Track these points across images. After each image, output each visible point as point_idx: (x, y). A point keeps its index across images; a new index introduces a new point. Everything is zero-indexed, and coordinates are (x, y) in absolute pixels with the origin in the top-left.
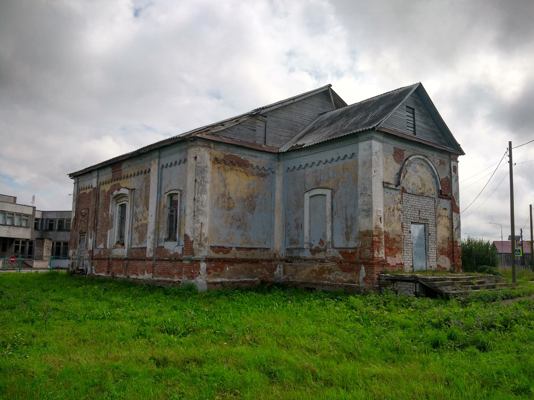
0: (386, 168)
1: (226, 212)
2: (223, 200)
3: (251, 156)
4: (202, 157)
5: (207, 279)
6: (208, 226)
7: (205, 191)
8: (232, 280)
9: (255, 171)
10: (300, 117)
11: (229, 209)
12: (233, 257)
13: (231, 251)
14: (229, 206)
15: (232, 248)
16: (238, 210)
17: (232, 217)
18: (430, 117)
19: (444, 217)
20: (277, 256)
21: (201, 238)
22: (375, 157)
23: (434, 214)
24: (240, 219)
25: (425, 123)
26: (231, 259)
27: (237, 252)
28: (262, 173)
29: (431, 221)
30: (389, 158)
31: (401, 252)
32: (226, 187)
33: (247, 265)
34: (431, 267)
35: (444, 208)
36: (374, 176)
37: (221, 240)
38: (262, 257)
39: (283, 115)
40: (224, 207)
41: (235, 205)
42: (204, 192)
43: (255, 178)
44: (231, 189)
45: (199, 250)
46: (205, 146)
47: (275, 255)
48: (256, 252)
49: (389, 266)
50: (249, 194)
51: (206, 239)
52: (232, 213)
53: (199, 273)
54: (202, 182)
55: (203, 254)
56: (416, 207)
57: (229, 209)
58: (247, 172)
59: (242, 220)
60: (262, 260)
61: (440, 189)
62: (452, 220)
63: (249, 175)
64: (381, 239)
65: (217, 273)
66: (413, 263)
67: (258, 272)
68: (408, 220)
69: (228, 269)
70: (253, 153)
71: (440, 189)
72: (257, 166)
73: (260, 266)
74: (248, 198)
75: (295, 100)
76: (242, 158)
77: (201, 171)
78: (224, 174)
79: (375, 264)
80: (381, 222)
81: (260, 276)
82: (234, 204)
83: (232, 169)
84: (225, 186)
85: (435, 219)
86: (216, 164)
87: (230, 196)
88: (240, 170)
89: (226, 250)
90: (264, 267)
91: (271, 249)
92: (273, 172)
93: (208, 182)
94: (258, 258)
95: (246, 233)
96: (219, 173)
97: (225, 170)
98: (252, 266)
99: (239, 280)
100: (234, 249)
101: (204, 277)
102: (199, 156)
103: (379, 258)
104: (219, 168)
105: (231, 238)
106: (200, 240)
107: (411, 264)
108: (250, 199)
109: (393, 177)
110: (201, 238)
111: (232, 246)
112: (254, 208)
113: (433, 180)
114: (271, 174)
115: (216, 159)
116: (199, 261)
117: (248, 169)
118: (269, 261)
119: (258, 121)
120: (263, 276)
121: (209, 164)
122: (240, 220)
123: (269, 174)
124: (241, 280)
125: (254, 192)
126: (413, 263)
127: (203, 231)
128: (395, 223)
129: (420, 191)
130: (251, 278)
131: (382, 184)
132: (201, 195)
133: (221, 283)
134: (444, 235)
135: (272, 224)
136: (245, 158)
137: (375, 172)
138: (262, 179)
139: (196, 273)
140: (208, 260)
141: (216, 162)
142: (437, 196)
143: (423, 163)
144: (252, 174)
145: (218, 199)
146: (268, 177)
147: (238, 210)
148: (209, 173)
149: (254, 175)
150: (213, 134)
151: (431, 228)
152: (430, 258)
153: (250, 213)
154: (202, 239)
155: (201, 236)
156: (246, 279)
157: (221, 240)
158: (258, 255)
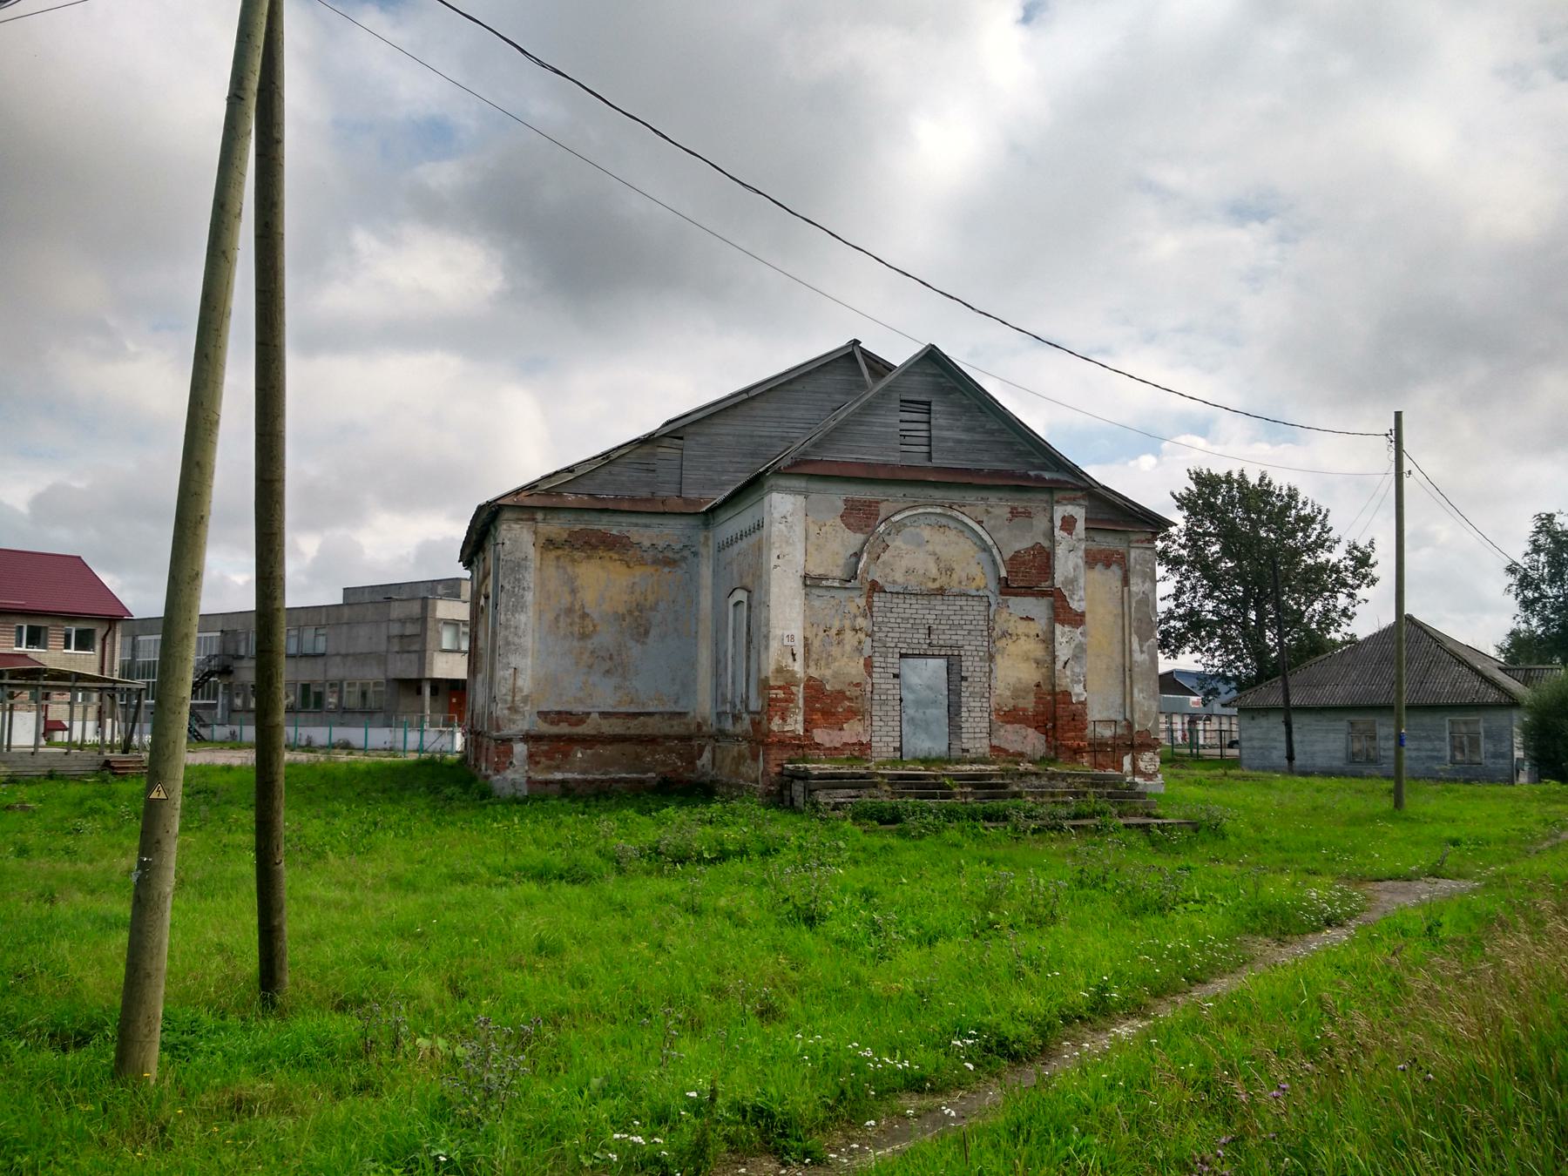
0: (818, 545)
1: (575, 643)
2: (569, 620)
3: (636, 525)
4: (516, 541)
5: (531, 774)
6: (529, 672)
7: (522, 607)
8: (590, 777)
9: (648, 556)
10: (776, 424)
11: (584, 636)
12: (593, 732)
13: (588, 721)
14: (584, 633)
15: (589, 714)
16: (606, 637)
17: (592, 652)
18: (989, 412)
19: (1023, 638)
20: (704, 728)
21: (514, 697)
22: (782, 527)
23: (985, 633)
24: (611, 655)
25: (969, 430)
26: (588, 735)
27: (604, 722)
28: (668, 557)
29: (972, 650)
30: (828, 524)
31: (864, 719)
32: (575, 595)
33: (628, 748)
34: (964, 750)
35: (1022, 618)
36: (776, 566)
37: (564, 698)
38: (667, 730)
39: (725, 430)
40: (572, 633)
41: (598, 628)
42: (519, 609)
43: (650, 570)
44: (589, 597)
45: (510, 720)
46: (522, 520)
47: (699, 726)
48: (650, 721)
49: (818, 749)
50: (634, 604)
51: (525, 700)
52: (590, 645)
53: (511, 763)
54: (516, 589)
55: (520, 727)
56: (917, 621)
57: (584, 636)
58: (628, 559)
59: (615, 657)
60: (667, 737)
61: (1003, 574)
62: (1054, 642)
63: (632, 565)
64: (793, 694)
65: (554, 763)
66: (901, 741)
67: (657, 760)
68: (891, 650)
69: (579, 755)
70: (634, 519)
71: (1003, 574)
72: (653, 545)
73: (659, 749)
74: (630, 612)
75: (752, 393)
76: (614, 532)
77: (512, 570)
78: (569, 569)
79: (771, 744)
80: (795, 660)
81: (662, 769)
82: (594, 626)
83: (589, 557)
84: (573, 591)
85: (986, 644)
86: (550, 550)
87: (587, 610)
88: (611, 558)
89: (574, 718)
90: (670, 751)
91: (692, 714)
92: (695, 554)
93: (529, 588)
94: (656, 732)
95: (627, 683)
96: (558, 567)
97: (573, 561)
98: (639, 749)
99: (608, 777)
100: (595, 716)
101: (521, 771)
102: (509, 539)
103: (783, 732)
104: (558, 558)
105: (590, 695)
106: (513, 701)
107: (898, 745)
108: (636, 613)
109: (841, 562)
110: (514, 697)
111: (590, 710)
112: (647, 633)
113: (984, 556)
114: (690, 556)
115: (550, 541)
116: (510, 740)
117: (630, 552)
118: (685, 739)
119: (660, 450)
120: (669, 769)
121: (532, 552)
122: (611, 658)
123: (684, 559)
124: (612, 776)
125: (646, 600)
126: (901, 741)
127: (520, 683)
128: (845, 659)
129: (936, 585)
130: (637, 773)
131: (800, 582)
132: (513, 615)
133: (563, 782)
134: (1019, 679)
135: (693, 664)
136: (620, 531)
137: (778, 557)
138: (666, 570)
139: (504, 763)
140: (527, 738)
141: (551, 547)
142: (997, 592)
143: (944, 521)
144: (642, 562)
145: (556, 618)
146: (684, 565)
147: (606, 637)
148: (531, 570)
149: (646, 564)
150: (548, 492)
151: (969, 666)
152: (964, 730)
153: (638, 641)
154: (517, 699)
155: (514, 692)
156: (624, 775)
157: (564, 698)
158: (653, 727)
